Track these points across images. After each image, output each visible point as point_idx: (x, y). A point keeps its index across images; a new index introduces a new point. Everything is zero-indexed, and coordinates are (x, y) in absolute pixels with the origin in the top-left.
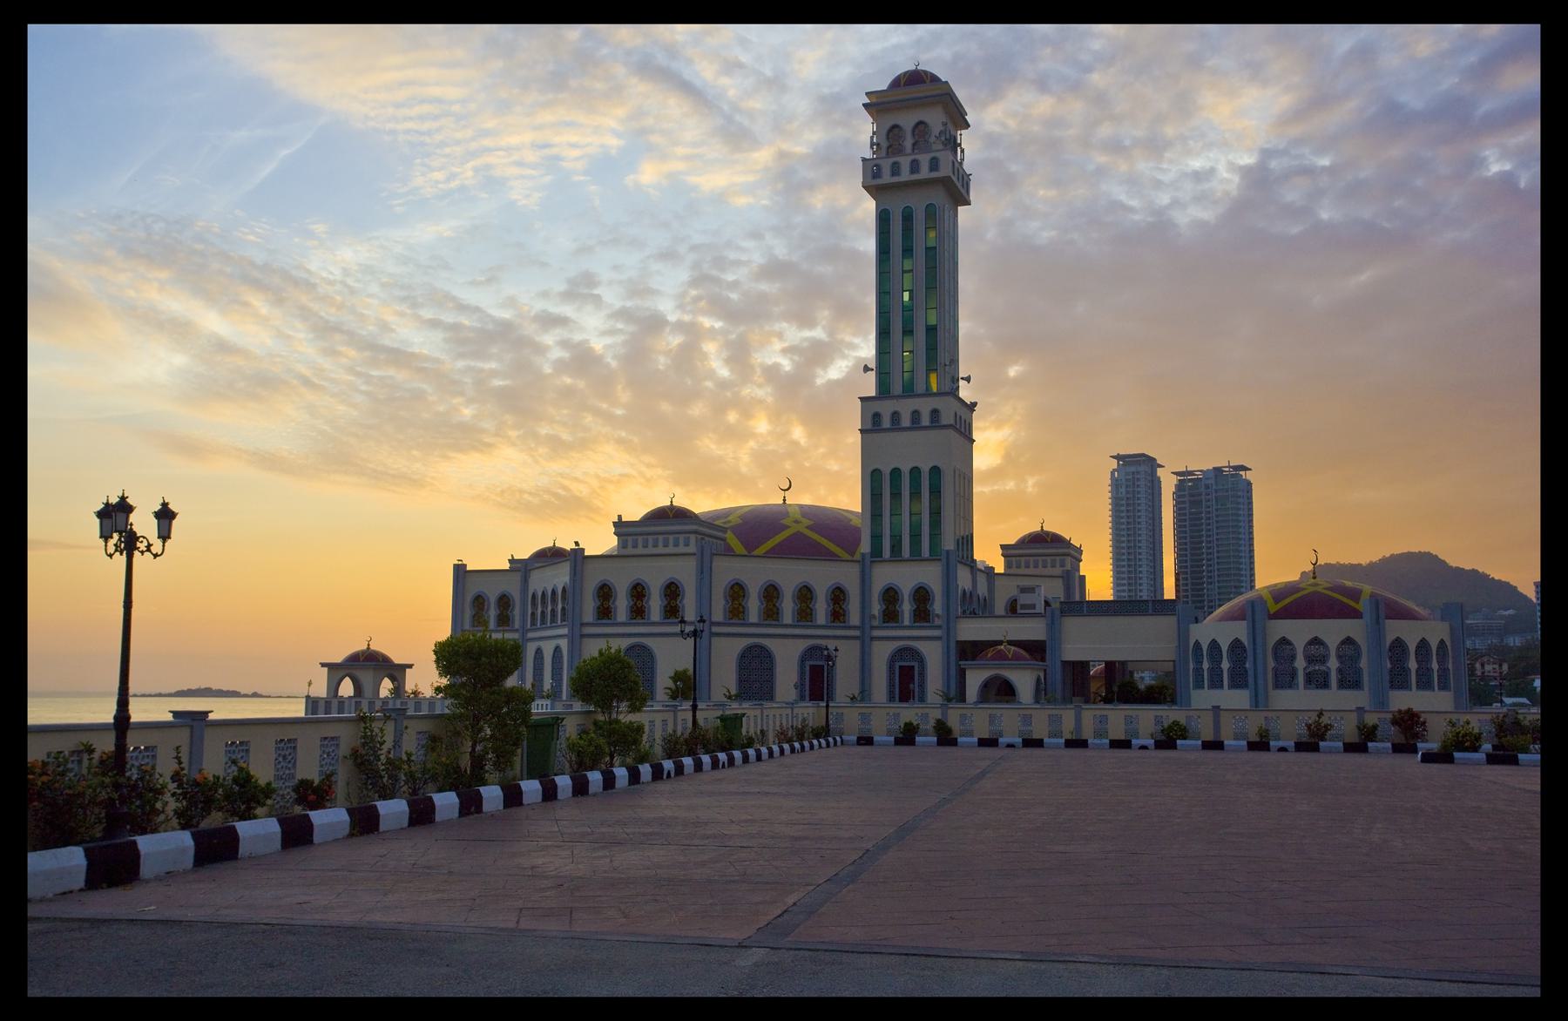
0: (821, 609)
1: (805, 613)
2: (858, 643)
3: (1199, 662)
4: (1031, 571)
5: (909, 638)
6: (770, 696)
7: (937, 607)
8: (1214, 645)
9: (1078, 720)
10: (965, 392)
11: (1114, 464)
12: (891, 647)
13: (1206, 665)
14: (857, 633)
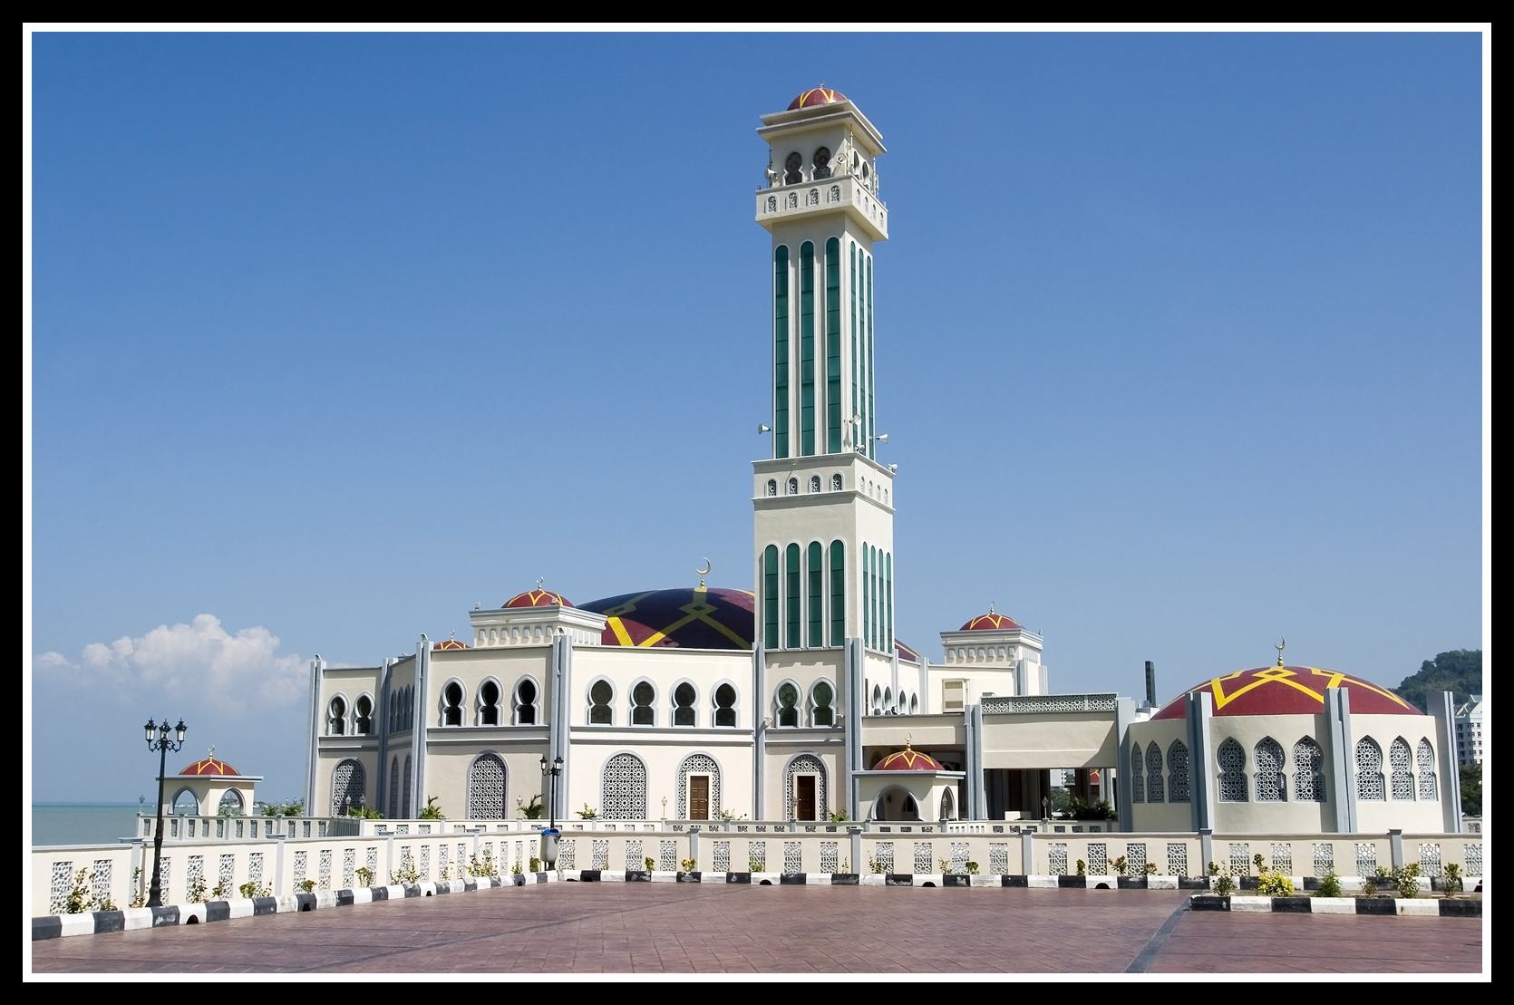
0: (704, 709)
1: (684, 714)
3: (1138, 770)
8: (1154, 748)
9: (693, 848)
13: (1145, 773)
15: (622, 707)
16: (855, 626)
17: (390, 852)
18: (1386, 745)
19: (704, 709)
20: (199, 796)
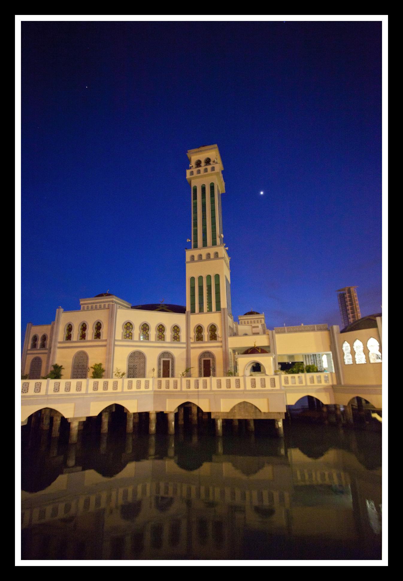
1: (161, 337)
5: (37, 354)
7: (219, 333)
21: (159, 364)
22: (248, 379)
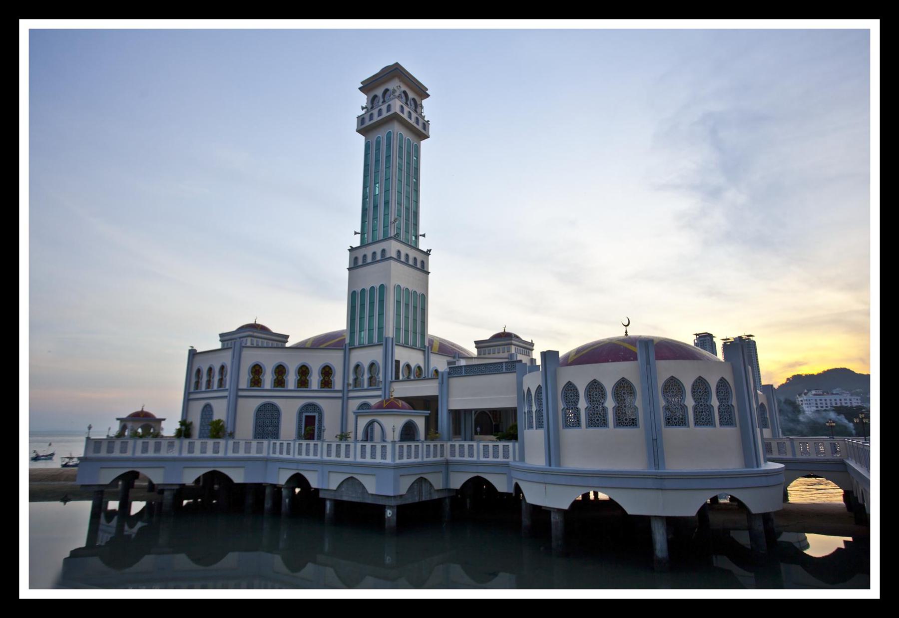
0: (315, 380)
2: (340, 401)
4: (496, 355)
6: (276, 435)
10: (423, 245)
11: (695, 337)
12: (359, 402)
13: (534, 409)
14: (340, 395)
15: (268, 379)
16: (390, 332)
17: (355, 447)
18: (609, 387)
19: (315, 380)
20: (142, 427)
21: (300, 420)
22: (334, 446)
